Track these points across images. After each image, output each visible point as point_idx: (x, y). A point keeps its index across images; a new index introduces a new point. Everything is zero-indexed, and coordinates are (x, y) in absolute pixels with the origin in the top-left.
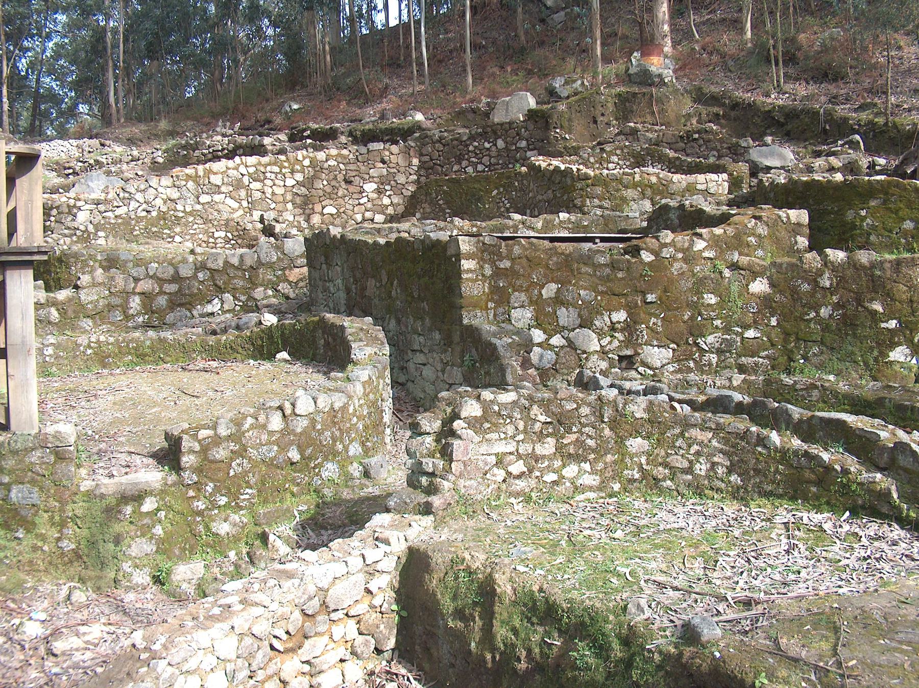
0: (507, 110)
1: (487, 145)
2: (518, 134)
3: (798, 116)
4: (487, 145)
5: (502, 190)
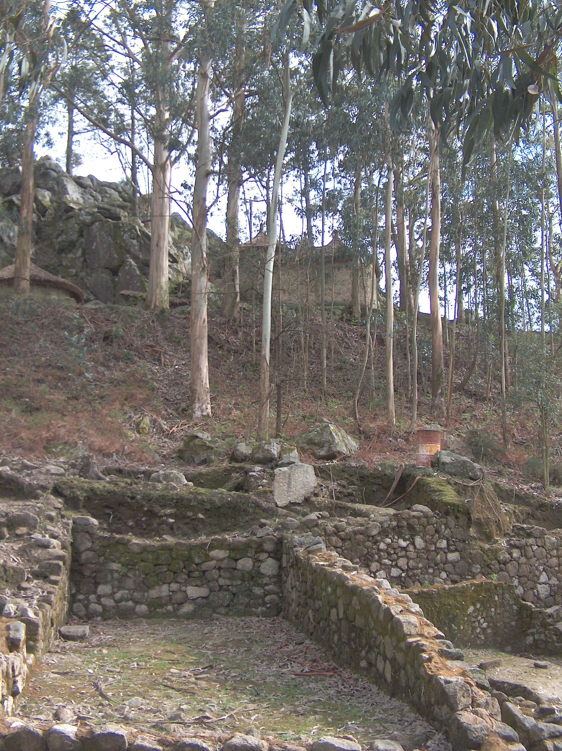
0: (289, 484)
1: (403, 544)
2: (437, 531)
4: (403, 544)
5: (478, 606)
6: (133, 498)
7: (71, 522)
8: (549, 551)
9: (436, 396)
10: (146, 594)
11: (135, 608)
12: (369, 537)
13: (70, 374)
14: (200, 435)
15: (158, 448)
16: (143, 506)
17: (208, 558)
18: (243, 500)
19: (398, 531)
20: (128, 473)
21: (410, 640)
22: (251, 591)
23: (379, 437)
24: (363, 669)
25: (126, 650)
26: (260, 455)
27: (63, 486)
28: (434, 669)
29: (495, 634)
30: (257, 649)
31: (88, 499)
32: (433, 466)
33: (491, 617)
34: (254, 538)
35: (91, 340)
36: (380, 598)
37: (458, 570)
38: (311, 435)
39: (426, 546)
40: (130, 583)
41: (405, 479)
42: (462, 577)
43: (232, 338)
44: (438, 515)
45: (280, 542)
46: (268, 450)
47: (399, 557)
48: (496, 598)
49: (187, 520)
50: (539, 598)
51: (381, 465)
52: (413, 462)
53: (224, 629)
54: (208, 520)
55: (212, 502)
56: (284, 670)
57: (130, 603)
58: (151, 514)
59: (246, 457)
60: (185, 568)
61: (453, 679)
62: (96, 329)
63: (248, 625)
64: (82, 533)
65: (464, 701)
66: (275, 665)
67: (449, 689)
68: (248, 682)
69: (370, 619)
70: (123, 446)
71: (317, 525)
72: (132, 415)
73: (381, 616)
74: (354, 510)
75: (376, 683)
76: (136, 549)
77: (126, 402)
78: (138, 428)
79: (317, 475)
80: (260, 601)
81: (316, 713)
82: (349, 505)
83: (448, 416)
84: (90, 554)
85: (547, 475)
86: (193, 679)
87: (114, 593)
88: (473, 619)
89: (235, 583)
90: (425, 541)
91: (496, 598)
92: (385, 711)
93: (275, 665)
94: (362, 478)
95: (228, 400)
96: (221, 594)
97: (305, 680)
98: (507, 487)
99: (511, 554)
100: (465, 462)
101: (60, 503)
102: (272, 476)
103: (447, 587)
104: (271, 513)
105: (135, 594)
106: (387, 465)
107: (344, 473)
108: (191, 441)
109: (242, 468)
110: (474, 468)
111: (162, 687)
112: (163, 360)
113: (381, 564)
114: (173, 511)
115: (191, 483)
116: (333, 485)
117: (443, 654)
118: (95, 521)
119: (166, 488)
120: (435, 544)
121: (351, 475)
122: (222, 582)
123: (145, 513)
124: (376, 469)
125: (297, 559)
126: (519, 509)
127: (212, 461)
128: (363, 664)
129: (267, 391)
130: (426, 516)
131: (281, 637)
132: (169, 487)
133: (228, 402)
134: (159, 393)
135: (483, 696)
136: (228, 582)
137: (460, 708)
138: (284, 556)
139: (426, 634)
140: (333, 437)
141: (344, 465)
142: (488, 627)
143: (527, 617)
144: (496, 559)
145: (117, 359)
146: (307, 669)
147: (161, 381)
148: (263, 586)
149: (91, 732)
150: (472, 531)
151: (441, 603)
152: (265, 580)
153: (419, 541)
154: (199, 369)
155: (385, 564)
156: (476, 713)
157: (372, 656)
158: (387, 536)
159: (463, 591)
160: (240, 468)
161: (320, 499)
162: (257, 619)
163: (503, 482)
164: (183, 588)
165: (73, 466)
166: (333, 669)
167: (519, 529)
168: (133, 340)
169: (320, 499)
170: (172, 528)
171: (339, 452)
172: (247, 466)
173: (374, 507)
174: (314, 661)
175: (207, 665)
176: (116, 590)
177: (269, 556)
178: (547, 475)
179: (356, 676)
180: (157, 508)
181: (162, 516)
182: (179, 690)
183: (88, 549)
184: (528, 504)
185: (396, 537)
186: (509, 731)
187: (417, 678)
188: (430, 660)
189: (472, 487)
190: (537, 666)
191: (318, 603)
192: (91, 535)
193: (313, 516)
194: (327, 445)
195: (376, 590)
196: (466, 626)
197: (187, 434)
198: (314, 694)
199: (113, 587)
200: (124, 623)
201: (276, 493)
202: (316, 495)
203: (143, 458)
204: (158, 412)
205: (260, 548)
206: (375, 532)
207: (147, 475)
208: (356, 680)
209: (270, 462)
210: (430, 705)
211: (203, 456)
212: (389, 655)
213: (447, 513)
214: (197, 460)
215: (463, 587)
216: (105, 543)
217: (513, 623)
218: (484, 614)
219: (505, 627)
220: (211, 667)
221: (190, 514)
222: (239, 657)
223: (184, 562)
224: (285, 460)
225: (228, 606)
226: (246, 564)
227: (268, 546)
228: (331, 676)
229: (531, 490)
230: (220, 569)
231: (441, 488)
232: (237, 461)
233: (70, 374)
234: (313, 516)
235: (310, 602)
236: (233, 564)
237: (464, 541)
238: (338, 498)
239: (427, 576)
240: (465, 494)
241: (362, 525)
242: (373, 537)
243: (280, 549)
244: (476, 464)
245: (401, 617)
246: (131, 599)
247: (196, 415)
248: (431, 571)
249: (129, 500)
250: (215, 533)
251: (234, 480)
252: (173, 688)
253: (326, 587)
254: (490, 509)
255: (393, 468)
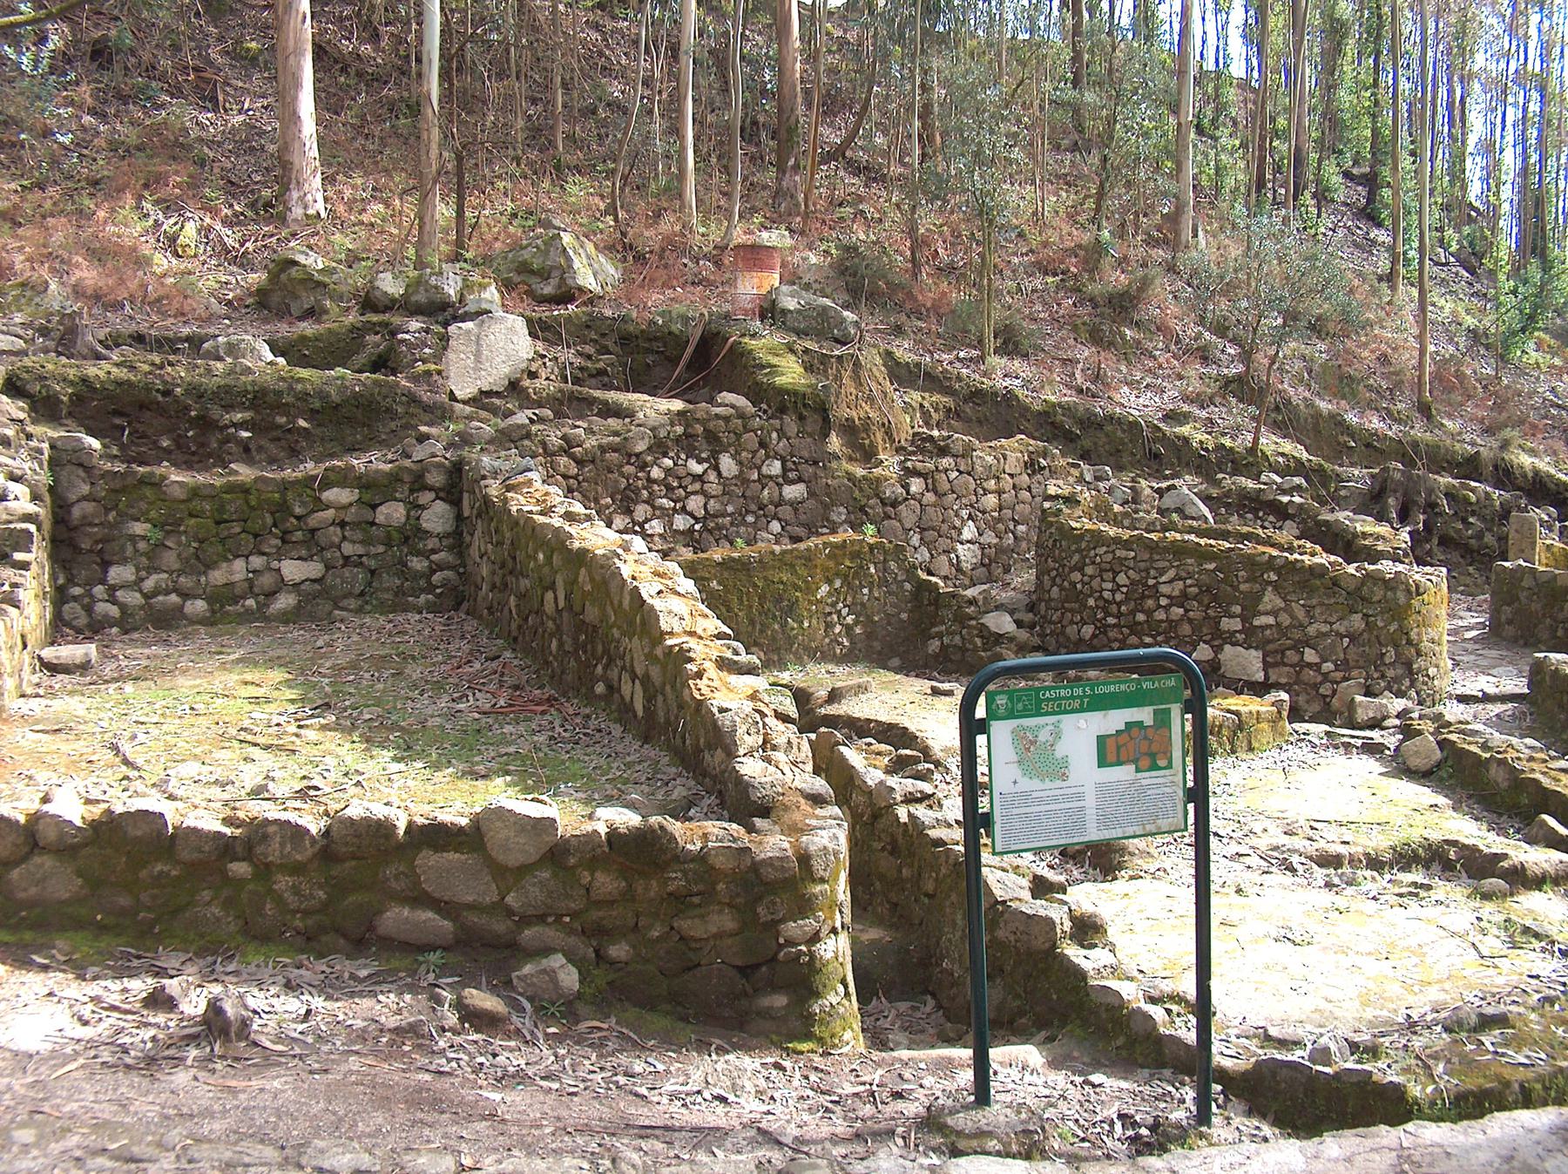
1: (696, 468)
3: (1100, 426)
4: (696, 468)
5: (838, 584)
6: (167, 393)
7: (45, 446)
8: (979, 482)
9: (784, 173)
10: (203, 579)
11: (183, 606)
12: (630, 456)
13: (23, 136)
14: (301, 259)
15: (217, 286)
16: (187, 408)
17: (321, 506)
18: (384, 390)
19: (687, 444)
20: (158, 341)
21: (669, 642)
22: (406, 565)
23: (661, 258)
24: (600, 697)
25: (168, 685)
26: (421, 297)
27: (25, 376)
28: (705, 690)
29: (869, 635)
30: (415, 671)
31: (78, 400)
32: (763, 318)
33: (863, 604)
34: (407, 463)
35: (62, 61)
36: (626, 571)
37: (803, 517)
38: (526, 255)
39: (741, 472)
40: (170, 559)
41: (711, 341)
42: (812, 531)
43: (366, 49)
44: (765, 412)
45: (457, 469)
46: (436, 287)
47: (688, 494)
48: (873, 570)
49: (278, 433)
50: (959, 569)
51: (662, 314)
52: (727, 307)
53: (355, 638)
54: (318, 431)
55: (322, 395)
56: (461, 706)
57: (174, 598)
58: (206, 424)
59: (394, 301)
60: (275, 525)
61: (732, 705)
62: (74, 35)
63: (400, 628)
64: (69, 467)
65: (747, 741)
66: (446, 698)
67: (725, 720)
68: (395, 727)
69: (609, 608)
70: (144, 286)
71: (528, 436)
72: (161, 216)
73: (626, 602)
74: (606, 403)
75: (619, 721)
76: (178, 493)
77: (146, 193)
78: (172, 244)
79: (533, 335)
80: (422, 583)
81: (507, 773)
82: (597, 393)
83: (806, 213)
84: (89, 507)
85: (989, 333)
86: (292, 729)
87: (142, 580)
88: (828, 610)
89: (373, 550)
90: (740, 463)
91: (873, 570)
92: (629, 765)
93: (446, 698)
94: (626, 340)
95: (359, 181)
96: (347, 572)
97: (496, 720)
98: (909, 358)
99: (906, 487)
100: (825, 308)
101: (22, 409)
102: (445, 339)
103: (777, 548)
104: (439, 414)
105: (182, 579)
106: (674, 315)
107: (592, 331)
108: (282, 270)
109: (386, 325)
110: (844, 320)
111: (236, 744)
112: (221, 98)
113: (653, 507)
114: (248, 415)
115: (281, 361)
116: (568, 355)
117: (723, 664)
118: (96, 444)
119: (231, 372)
120: (759, 468)
121: (603, 335)
122: (348, 549)
123: (193, 423)
124: (652, 322)
125: (486, 500)
126: (932, 399)
127: (326, 312)
128: (600, 688)
129: (434, 168)
130: (741, 415)
131: (461, 647)
132: (238, 369)
133: (356, 184)
134: (216, 170)
135: (782, 733)
136: (360, 550)
137: (741, 752)
138: (466, 495)
139: (700, 632)
140: (569, 259)
141: (590, 315)
142: (856, 622)
143: (930, 604)
144: (877, 496)
145: (124, 99)
146: (502, 703)
147: (219, 144)
148: (426, 554)
149: (109, 812)
150: (835, 443)
151: (766, 579)
152: (432, 543)
153: (727, 464)
154: (295, 118)
155: (661, 508)
156: (768, 760)
157: (614, 673)
158: (665, 455)
159: (808, 558)
160: (380, 324)
161: (540, 383)
162: (417, 617)
163: (904, 351)
164: (275, 564)
165: (44, 332)
166: (548, 700)
167: (923, 440)
168: (155, 56)
169: (540, 383)
170: (247, 450)
171: (581, 289)
172: (396, 320)
173: (646, 397)
174: (516, 688)
175: (320, 702)
176: (143, 573)
177: (437, 498)
178: (989, 333)
179: (587, 711)
180: (215, 412)
181: (227, 427)
182: (267, 748)
183: (84, 498)
184: (948, 391)
185: (683, 456)
186: (820, 785)
187: (681, 707)
188: (699, 675)
189: (840, 358)
190: (936, 692)
191: (525, 583)
192: (88, 469)
193: (521, 418)
194: (555, 273)
195: (618, 556)
196: (814, 621)
197: (275, 256)
198: (510, 744)
199: (138, 570)
200: (164, 636)
201: (453, 372)
202: (533, 375)
203: (187, 308)
204: (214, 212)
205: (418, 482)
206: (641, 447)
207: (195, 342)
208: (588, 717)
209: (443, 312)
210: (698, 751)
211: (308, 300)
212: (639, 671)
213: (782, 410)
214: (295, 311)
215: (808, 549)
216: (117, 484)
217: (904, 616)
218: (849, 599)
219: (889, 624)
220: (328, 705)
221: (282, 420)
222: (380, 686)
223: (272, 514)
224: (471, 308)
225: (362, 594)
226: (393, 513)
227: (435, 478)
228: (543, 713)
229: (958, 365)
230: (343, 524)
231: (774, 360)
232: (376, 310)
233: (23, 136)
234: (521, 418)
235: (511, 579)
236: (367, 514)
237: (816, 463)
238: (576, 381)
239: (742, 529)
240: (825, 371)
241: (616, 434)
242: (638, 455)
243: (457, 483)
244: (846, 313)
245: (657, 604)
246: (175, 590)
247: (294, 216)
248: (750, 519)
249: (160, 398)
250: (332, 456)
251: (369, 349)
252: (256, 745)
253: (536, 552)
254: (870, 399)
255: (685, 320)
